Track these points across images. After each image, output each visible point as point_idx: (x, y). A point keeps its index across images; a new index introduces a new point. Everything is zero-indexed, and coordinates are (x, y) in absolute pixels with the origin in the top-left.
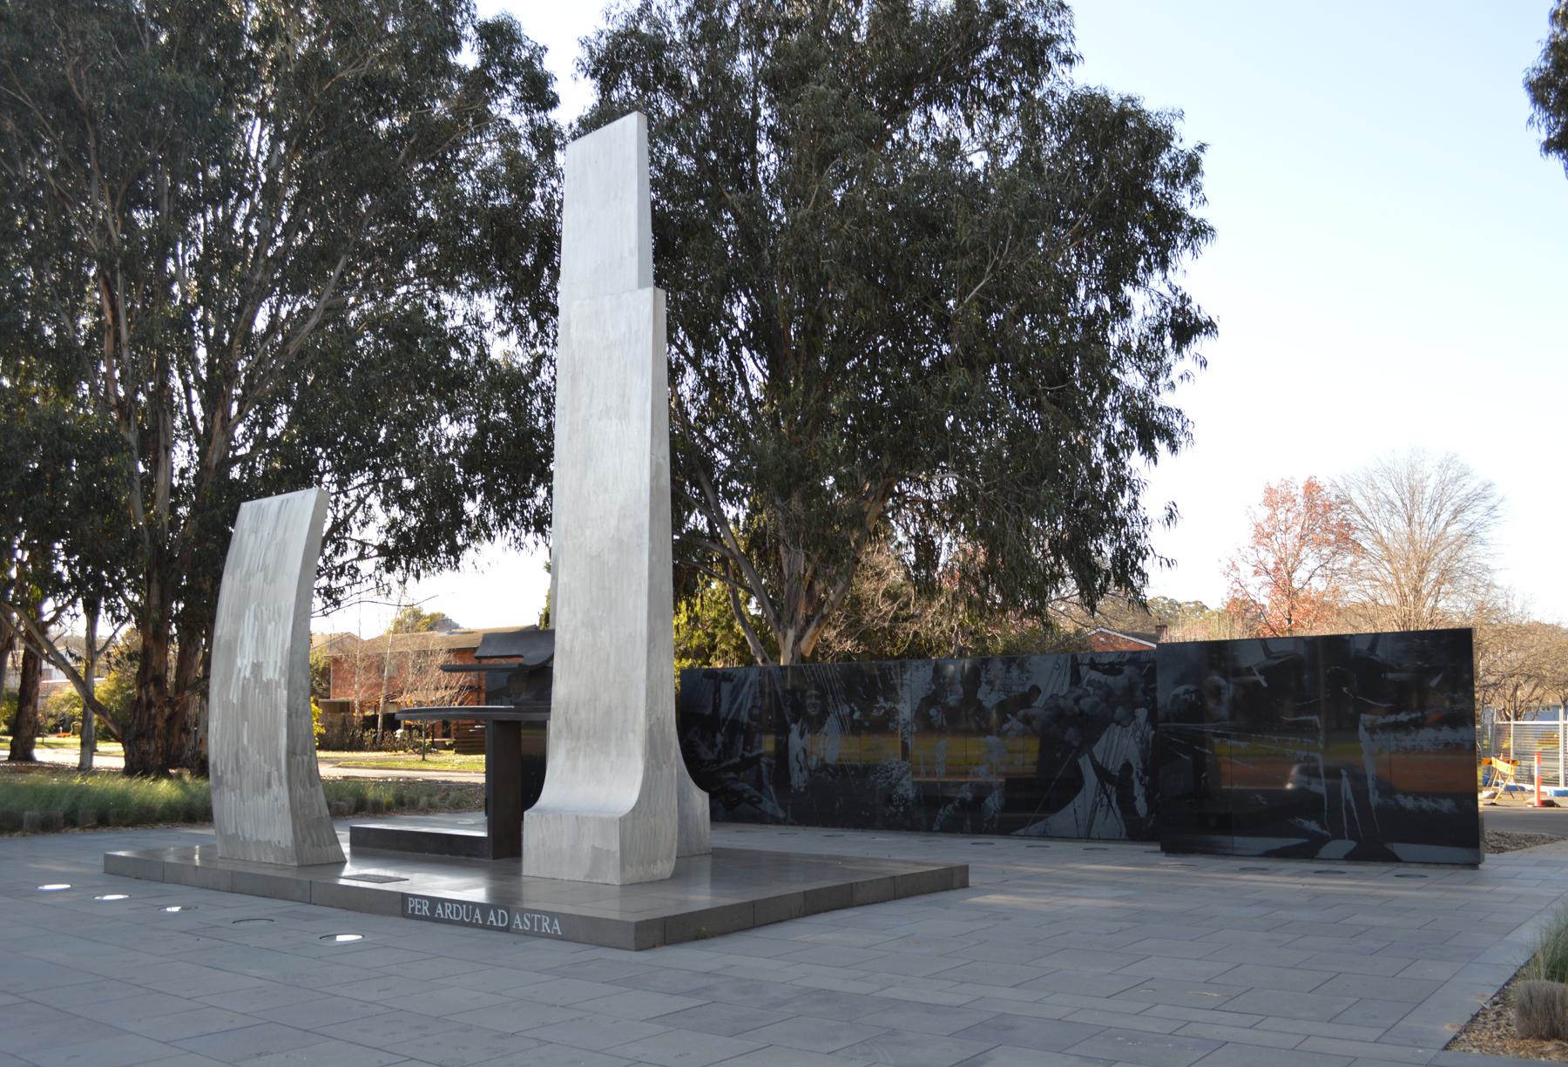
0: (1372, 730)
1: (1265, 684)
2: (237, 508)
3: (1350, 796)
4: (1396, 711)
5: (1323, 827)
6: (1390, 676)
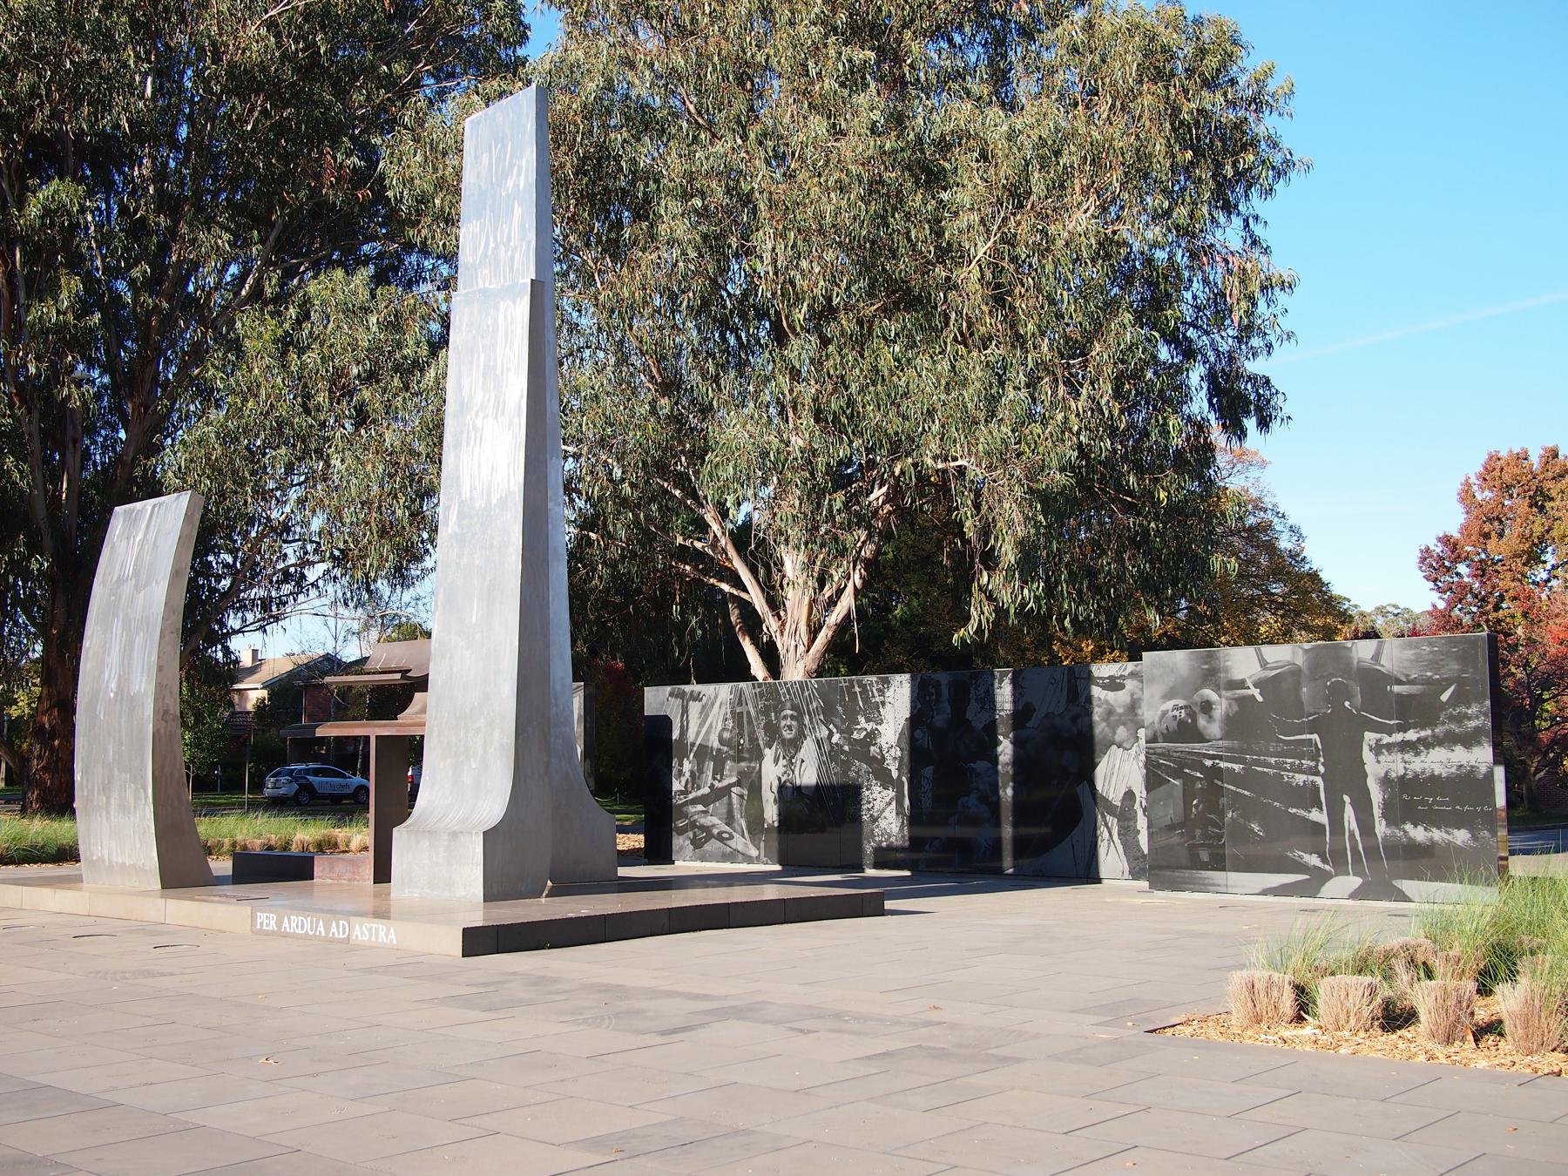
0: (1378, 749)
1: (1260, 699)
2: (110, 512)
3: (1354, 826)
4: (1403, 728)
5: (1325, 861)
6: (1397, 689)
